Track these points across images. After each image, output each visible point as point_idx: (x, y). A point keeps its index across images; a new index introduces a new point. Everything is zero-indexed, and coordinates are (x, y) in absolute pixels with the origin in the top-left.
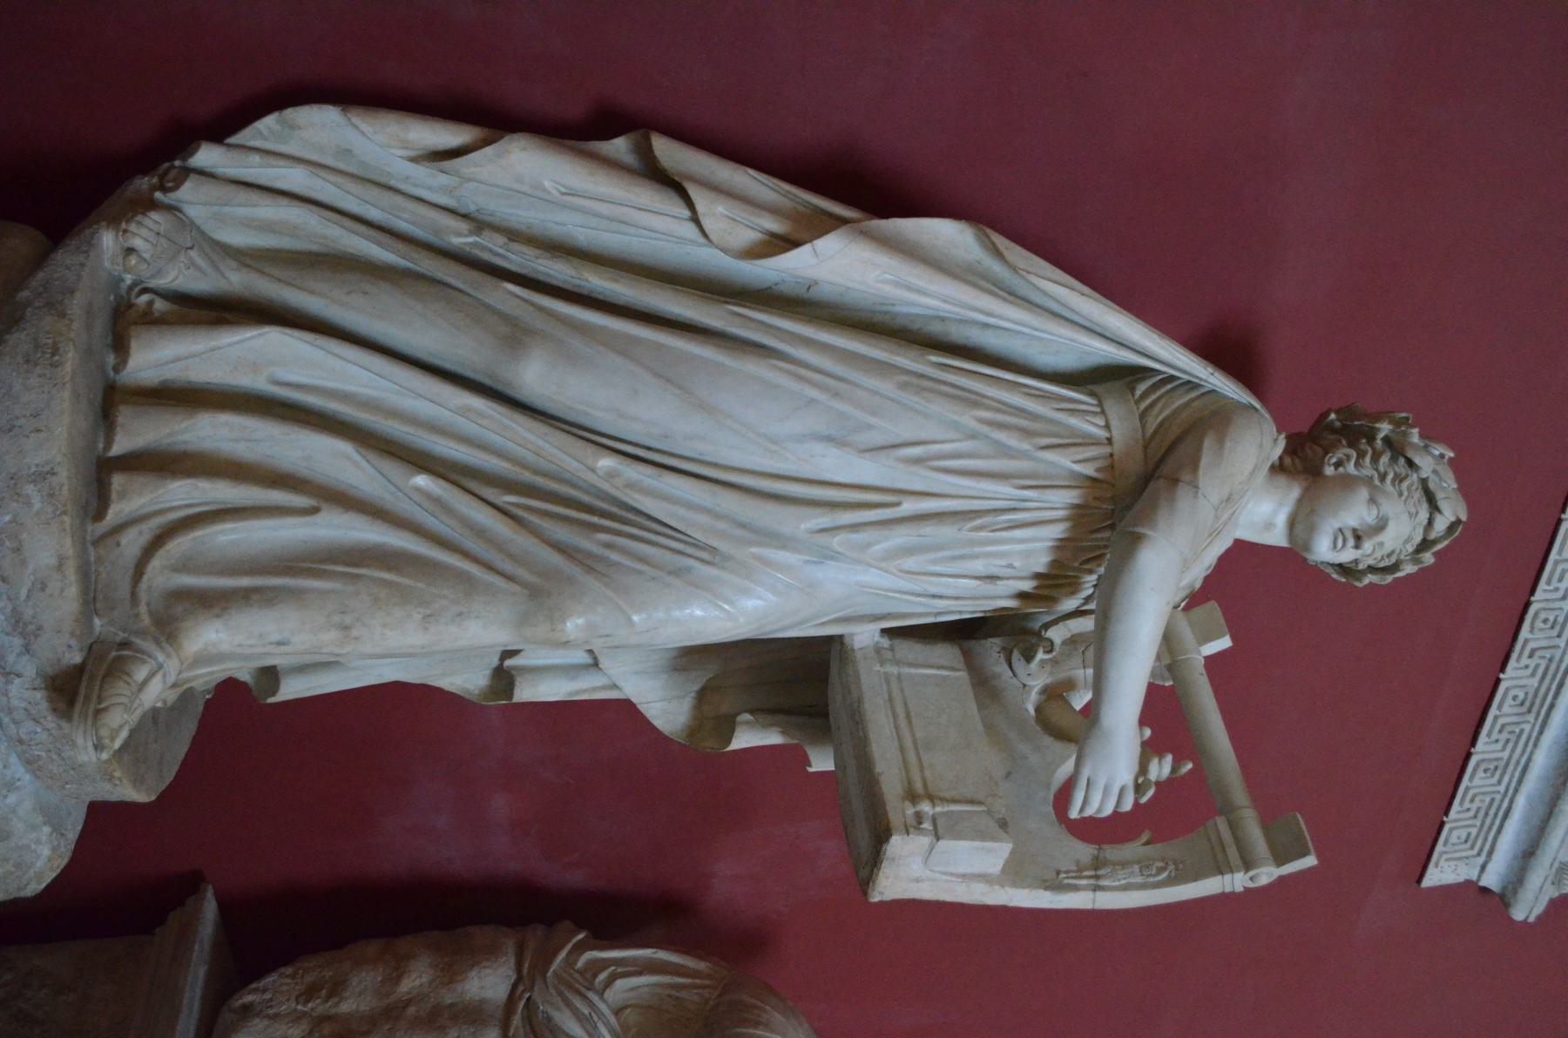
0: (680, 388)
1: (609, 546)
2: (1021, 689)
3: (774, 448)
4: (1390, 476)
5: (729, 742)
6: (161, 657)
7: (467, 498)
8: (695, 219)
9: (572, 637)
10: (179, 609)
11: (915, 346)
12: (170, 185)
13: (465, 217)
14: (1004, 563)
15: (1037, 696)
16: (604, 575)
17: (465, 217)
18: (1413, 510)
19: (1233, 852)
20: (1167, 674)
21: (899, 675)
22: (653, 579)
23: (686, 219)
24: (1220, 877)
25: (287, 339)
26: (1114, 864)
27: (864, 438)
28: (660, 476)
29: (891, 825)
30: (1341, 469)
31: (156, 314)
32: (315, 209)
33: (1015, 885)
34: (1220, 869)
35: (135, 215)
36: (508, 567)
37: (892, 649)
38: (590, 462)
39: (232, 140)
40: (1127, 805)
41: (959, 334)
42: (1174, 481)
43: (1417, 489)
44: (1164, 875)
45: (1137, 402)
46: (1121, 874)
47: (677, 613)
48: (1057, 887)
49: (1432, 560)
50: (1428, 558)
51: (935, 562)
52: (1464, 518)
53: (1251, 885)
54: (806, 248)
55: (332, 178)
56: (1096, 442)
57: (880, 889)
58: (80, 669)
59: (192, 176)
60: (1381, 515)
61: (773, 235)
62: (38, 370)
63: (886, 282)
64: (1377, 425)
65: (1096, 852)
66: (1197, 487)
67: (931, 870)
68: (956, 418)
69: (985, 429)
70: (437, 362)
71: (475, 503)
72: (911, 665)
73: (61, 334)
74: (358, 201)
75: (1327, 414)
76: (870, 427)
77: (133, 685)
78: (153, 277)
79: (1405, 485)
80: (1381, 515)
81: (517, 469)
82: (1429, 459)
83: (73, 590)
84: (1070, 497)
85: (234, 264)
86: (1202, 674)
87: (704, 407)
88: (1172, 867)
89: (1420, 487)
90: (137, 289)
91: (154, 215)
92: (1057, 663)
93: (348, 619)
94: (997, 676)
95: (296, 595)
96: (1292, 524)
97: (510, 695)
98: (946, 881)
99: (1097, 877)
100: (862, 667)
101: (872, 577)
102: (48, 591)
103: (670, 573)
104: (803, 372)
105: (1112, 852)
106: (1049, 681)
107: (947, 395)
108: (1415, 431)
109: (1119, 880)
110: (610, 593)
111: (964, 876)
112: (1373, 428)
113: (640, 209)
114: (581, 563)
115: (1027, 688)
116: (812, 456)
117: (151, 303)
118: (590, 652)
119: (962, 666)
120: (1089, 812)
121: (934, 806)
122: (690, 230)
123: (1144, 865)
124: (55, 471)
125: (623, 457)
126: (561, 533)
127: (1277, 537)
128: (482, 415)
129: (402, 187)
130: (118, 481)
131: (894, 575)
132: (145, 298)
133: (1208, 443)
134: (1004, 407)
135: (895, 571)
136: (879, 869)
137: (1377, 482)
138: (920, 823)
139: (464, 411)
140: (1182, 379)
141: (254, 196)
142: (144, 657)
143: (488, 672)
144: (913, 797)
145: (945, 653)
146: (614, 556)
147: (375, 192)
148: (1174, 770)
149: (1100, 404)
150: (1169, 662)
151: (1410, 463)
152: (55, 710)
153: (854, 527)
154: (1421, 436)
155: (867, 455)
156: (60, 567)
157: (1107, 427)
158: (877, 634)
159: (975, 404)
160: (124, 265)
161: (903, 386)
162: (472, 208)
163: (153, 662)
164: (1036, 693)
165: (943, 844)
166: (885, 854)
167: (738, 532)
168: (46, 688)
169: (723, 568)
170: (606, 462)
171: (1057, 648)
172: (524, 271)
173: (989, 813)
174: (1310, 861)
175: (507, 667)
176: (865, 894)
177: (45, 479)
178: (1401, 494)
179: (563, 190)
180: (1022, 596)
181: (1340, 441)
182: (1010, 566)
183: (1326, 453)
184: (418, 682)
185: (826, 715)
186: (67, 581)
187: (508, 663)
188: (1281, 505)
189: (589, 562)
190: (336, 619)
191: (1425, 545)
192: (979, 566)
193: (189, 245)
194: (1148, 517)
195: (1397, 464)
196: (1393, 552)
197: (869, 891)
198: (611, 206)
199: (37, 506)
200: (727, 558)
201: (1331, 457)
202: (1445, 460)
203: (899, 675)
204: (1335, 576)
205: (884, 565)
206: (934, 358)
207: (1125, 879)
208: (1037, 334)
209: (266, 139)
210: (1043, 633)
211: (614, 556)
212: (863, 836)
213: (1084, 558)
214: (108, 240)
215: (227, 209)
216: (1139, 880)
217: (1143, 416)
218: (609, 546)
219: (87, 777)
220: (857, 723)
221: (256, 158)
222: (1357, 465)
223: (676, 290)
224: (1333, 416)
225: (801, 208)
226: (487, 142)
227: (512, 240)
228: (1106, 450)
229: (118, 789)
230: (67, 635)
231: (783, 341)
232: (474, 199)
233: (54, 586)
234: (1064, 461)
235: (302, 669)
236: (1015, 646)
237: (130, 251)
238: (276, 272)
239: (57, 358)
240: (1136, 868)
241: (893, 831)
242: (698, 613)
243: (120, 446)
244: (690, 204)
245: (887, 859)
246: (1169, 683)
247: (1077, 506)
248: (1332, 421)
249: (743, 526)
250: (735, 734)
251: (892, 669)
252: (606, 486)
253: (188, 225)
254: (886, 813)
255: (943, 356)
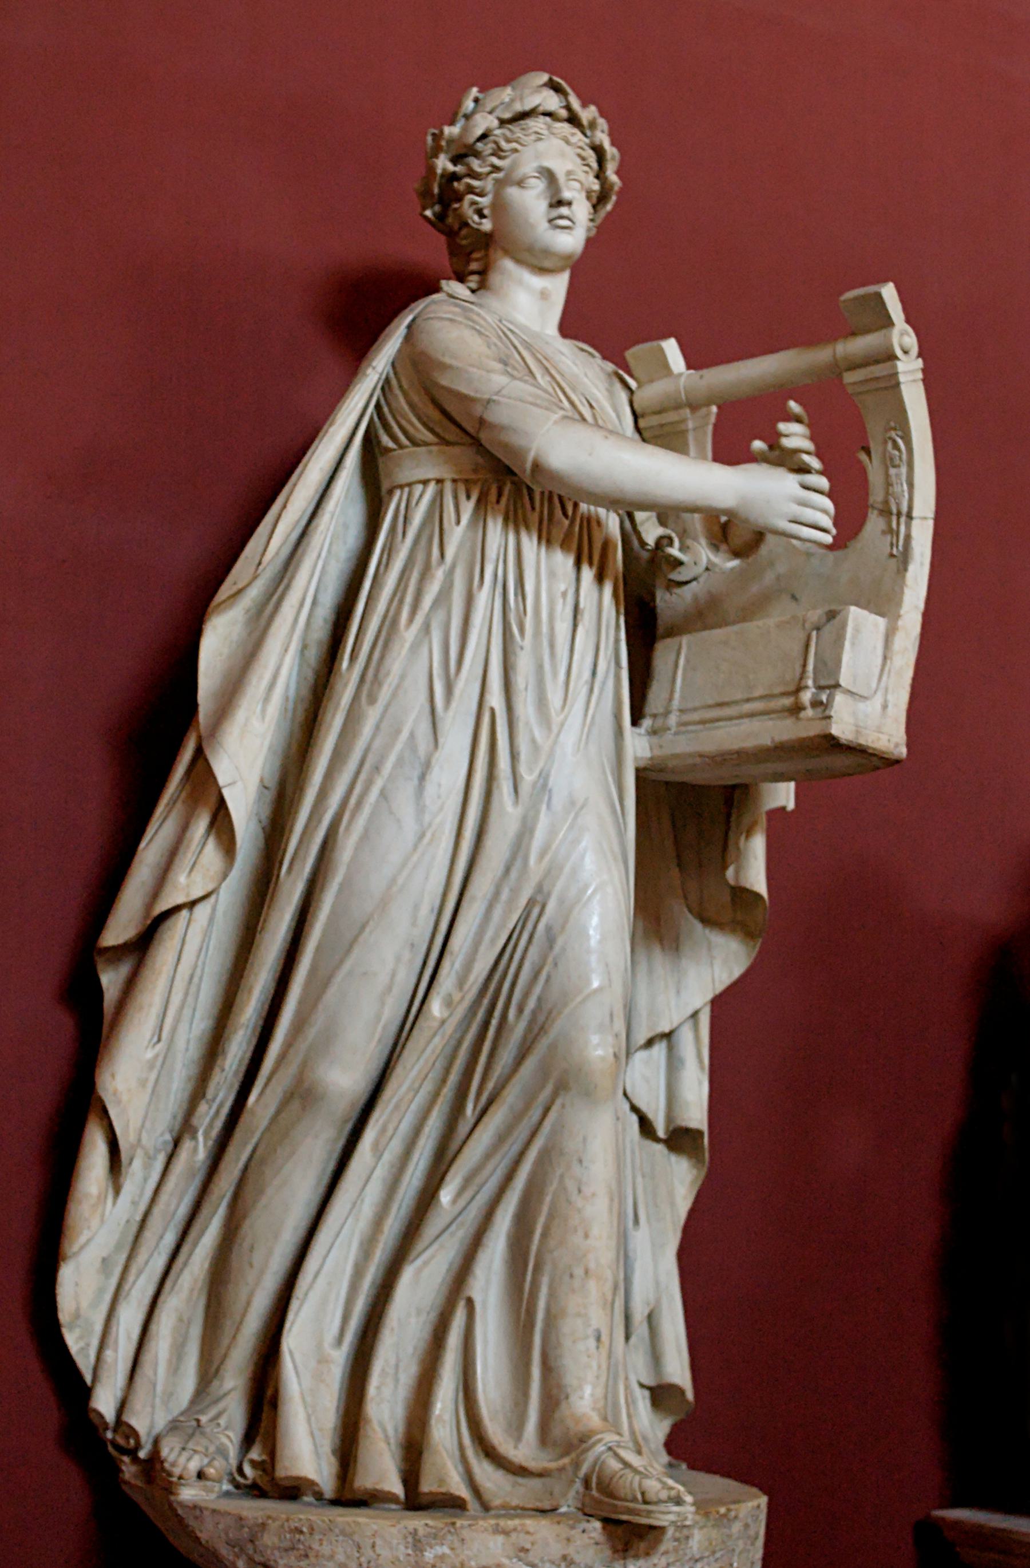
0: (363, 928)
1: (520, 1010)
2: (711, 573)
3: (428, 835)
4: (495, 161)
5: (758, 896)
6: (600, 1448)
7: (466, 1151)
8: (192, 905)
9: (611, 1051)
10: (557, 1432)
11: (331, 680)
12: (132, 1442)
13: (177, 1143)
14: (561, 601)
15: (720, 554)
16: (550, 1012)
17: (177, 1143)
18: (533, 137)
19: (878, 370)
20: (704, 410)
21: (682, 711)
22: (556, 965)
23: (191, 914)
24: (903, 387)
25: (296, 1329)
26: (887, 493)
27: (423, 743)
28: (452, 953)
29: (822, 733)
30: (486, 212)
31: (264, 1457)
32: (162, 1298)
33: (899, 604)
34: (893, 385)
35: (163, 1469)
36: (535, 1114)
37: (654, 716)
38: (436, 1024)
39: (88, 1379)
40: (823, 483)
41: (321, 631)
42: (482, 422)
43: (510, 130)
44: (900, 442)
45: (401, 446)
46: (897, 489)
47: (593, 942)
48: (904, 559)
49: (593, 109)
50: (588, 114)
51: (555, 674)
52: (545, 77)
53: (915, 350)
54: (226, 793)
55: (131, 1278)
56: (440, 495)
57: (892, 746)
58: (606, 1521)
59: (125, 1418)
60: (536, 175)
61: (212, 824)
62: (316, 1546)
63: (264, 711)
64: (439, 171)
65: (876, 512)
66: (489, 401)
67: (875, 692)
68: (407, 645)
69: (419, 619)
70: (326, 1180)
71: (471, 1143)
72: (671, 699)
73: (282, 1526)
74: (156, 1254)
75: (426, 218)
76: (412, 736)
77: (622, 1472)
78: (226, 1458)
79: (504, 144)
80: (536, 175)
81: (441, 1100)
82: (478, 117)
83: (530, 1523)
84: (495, 529)
85: (216, 1383)
86: (701, 377)
87: (384, 903)
88: (893, 434)
89: (510, 126)
90: (239, 1478)
91: (165, 1452)
92: (685, 531)
93: (579, 1272)
94: (696, 598)
95: (551, 1320)
96: (542, 270)
97: (699, 1133)
98: (889, 677)
99: (899, 514)
100: (667, 751)
101: (569, 738)
102: (528, 1546)
103: (551, 948)
104: (353, 801)
105: (876, 496)
106: (703, 541)
107: (382, 657)
108: (447, 130)
109: (903, 491)
110: (567, 1011)
111: (885, 658)
112: (442, 176)
113: (179, 960)
114: (538, 1035)
115: (709, 567)
116: (439, 797)
117: (254, 1464)
118: (650, 1043)
119: (676, 639)
120: (827, 522)
121: (807, 687)
122: (202, 911)
123: (889, 462)
124: (412, 1531)
125: (432, 991)
126: (506, 1056)
127: (558, 285)
128: (383, 1130)
129: (142, 1207)
130: (427, 1486)
131: (569, 713)
132: (248, 1470)
133: (444, 381)
134: (399, 595)
135: (562, 717)
136: (868, 747)
137: (500, 175)
138: (821, 703)
139: (378, 1151)
140: (372, 413)
141: (147, 1358)
142: (599, 1462)
143: (674, 1158)
144: (797, 709)
145: (663, 655)
146: (531, 1004)
147: (148, 1234)
148: (798, 420)
149: (401, 487)
150: (688, 411)
151: (484, 137)
152: (648, 1554)
153: (514, 756)
154: (452, 123)
155: (441, 740)
156: (506, 1533)
157: (425, 482)
158: (637, 730)
159: (395, 622)
160: (214, 1481)
161: (372, 700)
162: (168, 1137)
163: (603, 1457)
164: (716, 556)
165: (843, 682)
166: (851, 741)
167: (514, 874)
168: (625, 1558)
169: (549, 895)
170: (436, 1007)
171: (669, 532)
172: (236, 1086)
173: (818, 629)
174: (889, 292)
175: (666, 1133)
176: (898, 762)
177: (420, 1541)
178: (516, 151)
179: (155, 1039)
180: (600, 578)
181: (456, 209)
182: (564, 594)
183: (466, 224)
184: (679, 1235)
185: (734, 787)
186: (519, 1528)
187: (661, 1133)
188: (520, 282)
189: (536, 1030)
190: (577, 1283)
191: (573, 120)
192: (563, 628)
193: (194, 1423)
194: (518, 454)
195: (483, 151)
196: (579, 156)
197: (893, 758)
198: (174, 990)
199: (446, 1550)
200: (539, 889)
201: (474, 222)
202: (480, 96)
203: (681, 711)
204: (609, 207)
205: (555, 729)
206: (345, 664)
207: (902, 485)
208: (324, 554)
209: (88, 1345)
210: (649, 548)
211: (531, 1004)
212: (839, 762)
213: (560, 513)
214: (188, 1494)
215: (159, 1388)
216: (904, 470)
217: (415, 443)
218: (520, 1010)
219: (723, 1542)
220: (725, 760)
221: (109, 1354)
222: (481, 195)
223: (263, 928)
224: (428, 213)
225: (184, 795)
226: (105, 1112)
227: (204, 1095)
228: (448, 487)
229: (741, 1515)
230: (573, 1532)
231: (320, 821)
232: (159, 1134)
233: (525, 1542)
234: (456, 535)
235: (656, 1357)
236: (665, 576)
237: (201, 1475)
238: (225, 1342)
239: (305, 1529)
240: (892, 471)
241: (827, 732)
242: (595, 920)
243: (396, 1487)
244: (176, 909)
245: (857, 738)
246: (714, 409)
247: (506, 520)
248: (434, 214)
249: (507, 870)
250: (748, 886)
251: (673, 720)
252: (460, 1011)
253: (174, 1426)
254: (811, 739)
255: (344, 652)
